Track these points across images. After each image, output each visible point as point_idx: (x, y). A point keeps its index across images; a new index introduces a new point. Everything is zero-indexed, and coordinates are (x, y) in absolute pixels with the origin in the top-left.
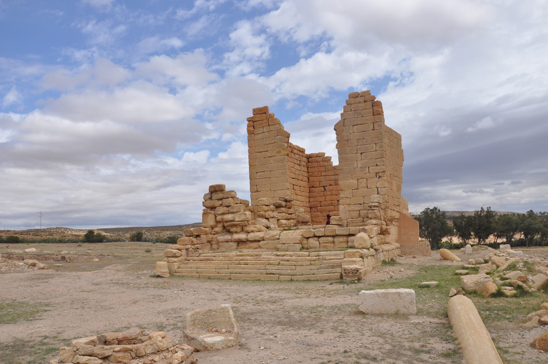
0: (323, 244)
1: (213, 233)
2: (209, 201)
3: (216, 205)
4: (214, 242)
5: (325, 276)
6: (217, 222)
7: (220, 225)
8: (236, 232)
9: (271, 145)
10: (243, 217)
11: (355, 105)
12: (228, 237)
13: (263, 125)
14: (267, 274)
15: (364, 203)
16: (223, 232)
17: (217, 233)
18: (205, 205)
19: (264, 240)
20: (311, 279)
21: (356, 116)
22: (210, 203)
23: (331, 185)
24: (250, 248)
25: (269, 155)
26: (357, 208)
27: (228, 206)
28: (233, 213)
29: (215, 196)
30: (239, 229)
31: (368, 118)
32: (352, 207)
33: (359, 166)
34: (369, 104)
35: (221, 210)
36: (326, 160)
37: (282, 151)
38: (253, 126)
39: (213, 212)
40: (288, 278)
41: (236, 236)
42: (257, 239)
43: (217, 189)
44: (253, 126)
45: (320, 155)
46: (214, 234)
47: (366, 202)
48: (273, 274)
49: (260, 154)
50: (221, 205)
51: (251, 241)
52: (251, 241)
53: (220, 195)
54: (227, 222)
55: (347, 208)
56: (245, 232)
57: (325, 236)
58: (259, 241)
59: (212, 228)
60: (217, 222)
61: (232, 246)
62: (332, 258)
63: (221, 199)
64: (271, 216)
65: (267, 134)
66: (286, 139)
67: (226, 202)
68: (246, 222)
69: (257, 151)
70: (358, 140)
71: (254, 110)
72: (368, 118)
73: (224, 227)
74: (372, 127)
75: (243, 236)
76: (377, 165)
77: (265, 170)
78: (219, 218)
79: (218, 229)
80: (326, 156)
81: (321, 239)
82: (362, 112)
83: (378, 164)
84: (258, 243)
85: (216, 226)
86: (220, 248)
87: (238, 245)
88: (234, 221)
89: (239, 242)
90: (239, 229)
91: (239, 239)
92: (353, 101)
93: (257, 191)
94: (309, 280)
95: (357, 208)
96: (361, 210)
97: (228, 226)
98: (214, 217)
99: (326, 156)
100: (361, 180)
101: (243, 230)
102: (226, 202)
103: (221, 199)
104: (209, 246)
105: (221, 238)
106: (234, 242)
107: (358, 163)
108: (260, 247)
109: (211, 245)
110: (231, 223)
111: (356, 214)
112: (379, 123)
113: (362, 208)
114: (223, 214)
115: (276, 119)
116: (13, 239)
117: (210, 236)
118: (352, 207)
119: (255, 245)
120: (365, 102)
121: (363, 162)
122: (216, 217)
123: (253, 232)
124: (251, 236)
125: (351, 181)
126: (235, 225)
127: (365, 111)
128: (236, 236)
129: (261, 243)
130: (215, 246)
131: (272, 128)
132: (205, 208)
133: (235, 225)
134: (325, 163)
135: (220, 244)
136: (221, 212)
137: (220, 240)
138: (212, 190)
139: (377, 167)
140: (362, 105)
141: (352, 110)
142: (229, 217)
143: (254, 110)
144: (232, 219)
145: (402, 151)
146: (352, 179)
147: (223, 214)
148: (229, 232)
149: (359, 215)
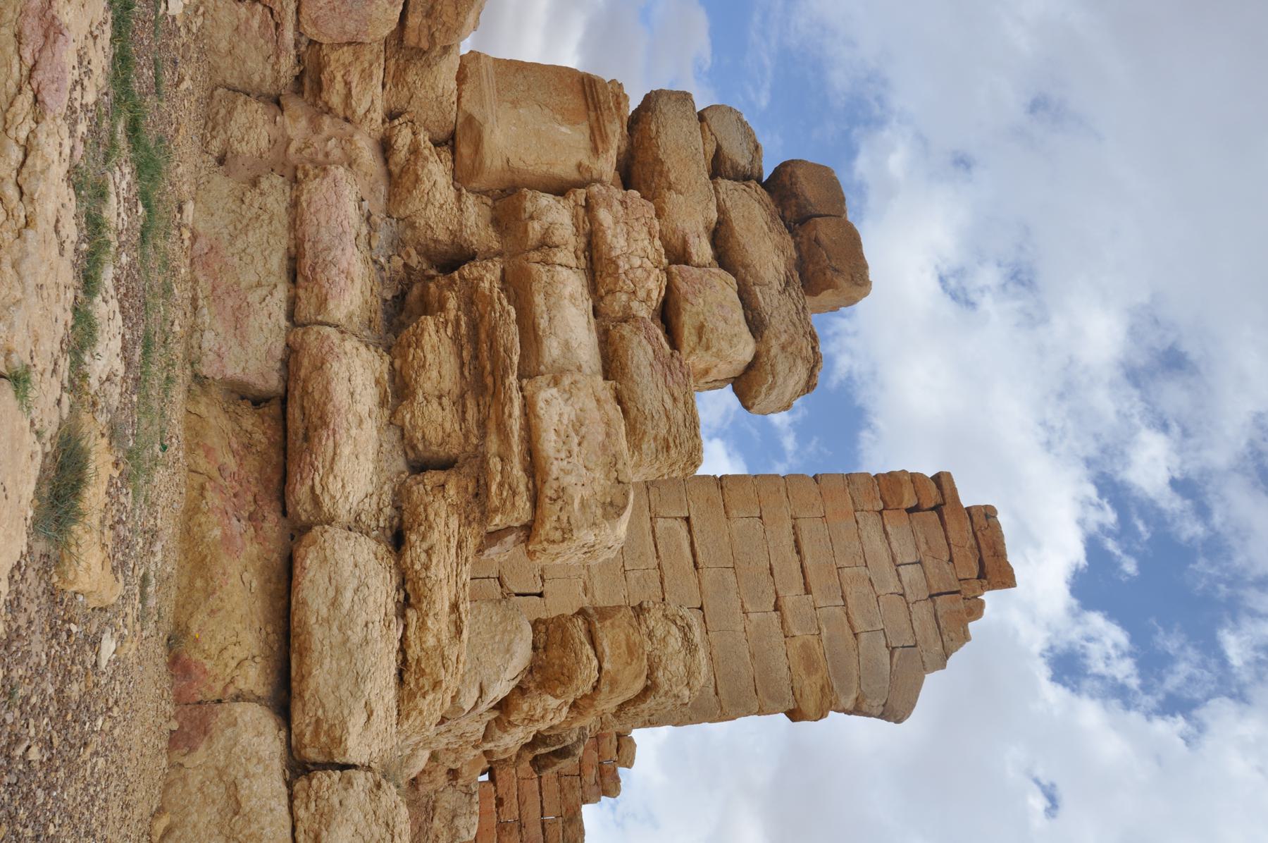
1: (403, 139)
2: (701, 150)
4: (296, 125)
6: (506, 202)
7: (474, 221)
8: (399, 390)
10: (576, 474)
12: (352, 292)
13: (929, 562)
16: (398, 244)
17: (398, 179)
18: (667, 109)
19: (299, 768)
22: (681, 150)
23: (500, 802)
24: (198, 560)
27: (667, 315)
30: (436, 421)
35: (632, 240)
36: (607, 780)
37: (817, 679)
39: (607, 166)
41: (354, 377)
42: (321, 676)
43: (824, 230)
45: (624, 751)
46: (385, 147)
49: (788, 541)
50: (678, 255)
51: (283, 581)
52: (283, 581)
53: (767, 252)
54: (518, 287)
56: (400, 498)
58: (283, 698)
59: (448, 142)
60: (506, 202)
61: (238, 321)
64: (46, 96)
65: (893, 586)
66: (877, 703)
67: (712, 300)
68: (522, 510)
69: (802, 524)
73: (453, 259)
75: (355, 468)
77: (708, 575)
79: (441, 203)
80: (622, 771)
84: (254, 678)
85: (461, 178)
86: (222, 186)
87: (244, 396)
88: (526, 373)
89: (283, 418)
90: (436, 421)
91: (317, 421)
97: (472, 298)
98: (565, 168)
99: (622, 771)
101: (419, 466)
104: (258, 69)
105: (345, 205)
106: (290, 358)
108: (192, 722)
109: (277, 102)
110: (511, 335)
114: (596, 265)
117: (371, 99)
119: (234, 642)
122: (560, 189)
123: (409, 598)
124: (349, 577)
128: (354, 377)
129: (255, 736)
130: (252, 130)
131: (922, 612)
132: (634, 103)
133: (481, 381)
134: (591, 775)
135: (274, 186)
137: (316, 190)
138: (809, 190)
142: (570, 325)
143: (989, 513)
144: (552, 349)
147: (596, 265)
148: (399, 314)
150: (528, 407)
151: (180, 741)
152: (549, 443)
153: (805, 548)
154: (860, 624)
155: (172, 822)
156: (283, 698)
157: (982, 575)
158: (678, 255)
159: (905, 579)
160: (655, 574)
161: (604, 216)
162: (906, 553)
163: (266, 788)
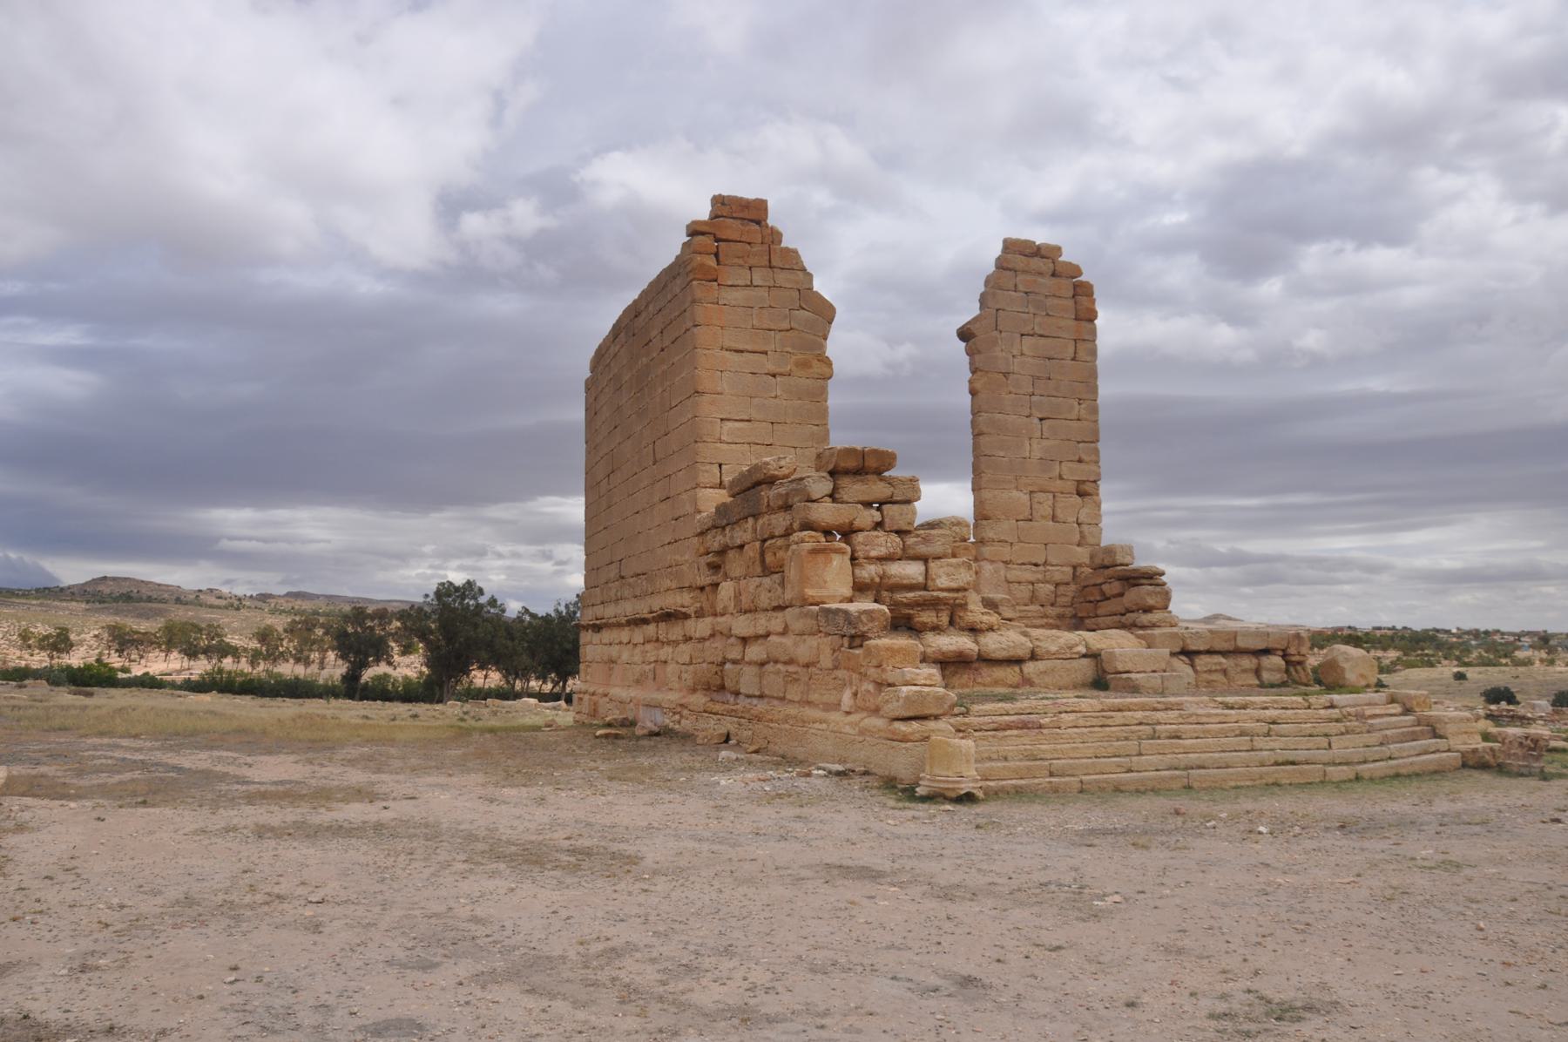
0: (1205, 676)
3: (857, 523)
5: (1431, 761)
8: (936, 629)
9: (779, 336)
11: (1029, 277)
13: (752, 261)
14: (1277, 764)
15: (1045, 563)
20: (1403, 771)
25: (771, 367)
26: (1028, 574)
29: (854, 489)
31: (1062, 323)
32: (1016, 573)
33: (1037, 454)
34: (1066, 287)
38: (716, 255)
40: (1346, 772)
44: (716, 255)
47: (1052, 560)
48: (1293, 763)
50: (879, 525)
53: (878, 490)
55: (1002, 573)
57: (1209, 652)
62: (1378, 711)
69: (727, 344)
70: (1035, 378)
71: (719, 201)
72: (1062, 323)
74: (1071, 350)
76: (1080, 461)
77: (754, 415)
78: (869, 572)
81: (1202, 661)
82: (1036, 304)
83: (1084, 457)
89: (952, 664)
92: (1019, 261)
94: (1397, 776)
95: (1028, 574)
96: (1039, 581)
100: (1040, 496)
107: (1035, 446)
111: (1023, 592)
113: (1040, 576)
115: (787, 250)
116: (11, 593)
118: (1016, 573)
119: (1010, 674)
120: (1053, 275)
121: (1045, 443)
125: (1015, 494)
126: (934, 604)
127: (1056, 301)
129: (1030, 668)
131: (781, 278)
133: (934, 604)
136: (882, 551)
139: (1082, 466)
140: (1047, 281)
141: (1021, 287)
142: (912, 571)
143: (719, 201)
145: (826, 409)
146: (1017, 488)
149: (1033, 599)
150: (942, 590)
151: (1032, 684)
152: (954, 585)
153: (741, 347)
154: (785, 325)
155: (718, 750)
156: (1019, 661)
157: (758, 223)
158: (879, 525)
159: (760, 283)
160: (754, 447)
161: (873, 554)
162: (742, 277)
163: (1041, 665)
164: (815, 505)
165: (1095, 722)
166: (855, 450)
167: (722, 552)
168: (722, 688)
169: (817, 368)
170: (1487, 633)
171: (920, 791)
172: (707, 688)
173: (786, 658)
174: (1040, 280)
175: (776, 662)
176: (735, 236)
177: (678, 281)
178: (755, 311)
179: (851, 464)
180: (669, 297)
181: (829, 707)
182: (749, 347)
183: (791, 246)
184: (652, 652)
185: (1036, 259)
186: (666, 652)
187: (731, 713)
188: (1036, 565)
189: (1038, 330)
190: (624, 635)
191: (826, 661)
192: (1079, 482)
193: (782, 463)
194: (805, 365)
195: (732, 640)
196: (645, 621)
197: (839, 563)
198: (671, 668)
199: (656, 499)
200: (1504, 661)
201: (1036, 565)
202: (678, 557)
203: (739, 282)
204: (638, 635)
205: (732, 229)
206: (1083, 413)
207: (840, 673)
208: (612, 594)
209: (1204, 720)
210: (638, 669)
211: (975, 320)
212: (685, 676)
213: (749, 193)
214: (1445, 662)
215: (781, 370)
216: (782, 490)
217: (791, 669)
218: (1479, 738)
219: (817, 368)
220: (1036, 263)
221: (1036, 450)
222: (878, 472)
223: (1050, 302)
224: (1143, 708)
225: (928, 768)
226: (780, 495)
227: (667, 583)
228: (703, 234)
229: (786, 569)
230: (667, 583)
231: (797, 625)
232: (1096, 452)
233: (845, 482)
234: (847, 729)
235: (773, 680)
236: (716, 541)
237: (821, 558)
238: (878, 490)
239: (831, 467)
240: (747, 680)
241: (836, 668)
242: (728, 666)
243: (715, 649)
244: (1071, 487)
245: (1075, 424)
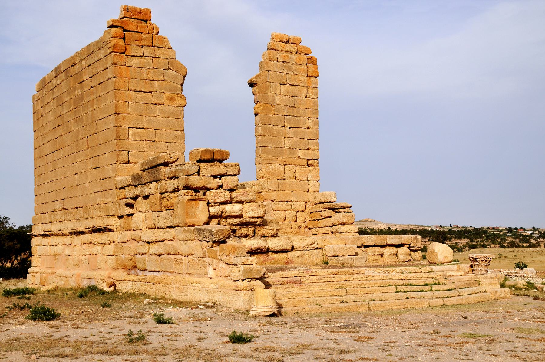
11: (285, 54)
13: (143, 43)
21: (285, 71)
28: (242, 202)
29: (207, 169)
31: (301, 78)
33: (287, 146)
34: (303, 59)
44: (124, 38)
53: (220, 169)
57: (374, 246)
62: (453, 274)
63: (220, 176)
74: (305, 92)
76: (308, 149)
78: (215, 210)
83: (310, 147)
92: (280, 46)
93: (128, 162)
102: (228, 181)
103: (220, 176)
112: (314, 90)
115: (162, 38)
120: (296, 53)
125: (277, 166)
136: (222, 200)
141: (280, 59)
143: (127, 9)
153: (138, 90)
156: (285, 251)
157: (146, 21)
160: (146, 142)
161: (218, 201)
162: (137, 51)
164: (191, 177)
165: (325, 280)
166: (210, 150)
167: (136, 198)
168: (135, 267)
169: (178, 101)
170: (516, 229)
171: (252, 313)
172: (125, 268)
173: (175, 252)
174: (290, 55)
175: (169, 254)
176: (134, 29)
177: (102, 51)
178: (145, 70)
179: (208, 157)
180: (96, 59)
181: (200, 276)
182: (143, 90)
183: (164, 36)
184: (87, 249)
185: (289, 45)
186: (97, 249)
187: (141, 280)
188: (287, 202)
189: (288, 82)
190: (68, 240)
191: (199, 253)
192: (309, 160)
193: (172, 155)
194: (171, 99)
195: (141, 243)
196: (82, 233)
197: (202, 205)
198: (99, 258)
199: (90, 168)
200: (525, 245)
201: (287, 202)
202: (104, 199)
203: (137, 54)
204: (77, 240)
205: (132, 25)
206: (311, 125)
207: (207, 259)
208: (58, 218)
209: (375, 278)
210: (76, 258)
211: (258, 76)
212: (109, 261)
213: (142, 6)
214: (492, 246)
215: (160, 102)
216: (173, 169)
217: (177, 257)
218: (499, 286)
219: (178, 101)
220: (289, 47)
221: (287, 144)
222: (220, 161)
223: (294, 67)
224: (346, 273)
225: (255, 303)
226: (172, 172)
227: (98, 213)
228: (116, 27)
229: (175, 208)
230: (98, 213)
231: (183, 236)
232: (317, 144)
233: (203, 165)
234: (212, 286)
235: (168, 262)
236: (132, 192)
237: (194, 203)
238: (220, 169)
239: (198, 159)
240: (151, 263)
241: (204, 257)
242: (138, 256)
243: (132, 246)
244: (304, 162)
245: (307, 130)
